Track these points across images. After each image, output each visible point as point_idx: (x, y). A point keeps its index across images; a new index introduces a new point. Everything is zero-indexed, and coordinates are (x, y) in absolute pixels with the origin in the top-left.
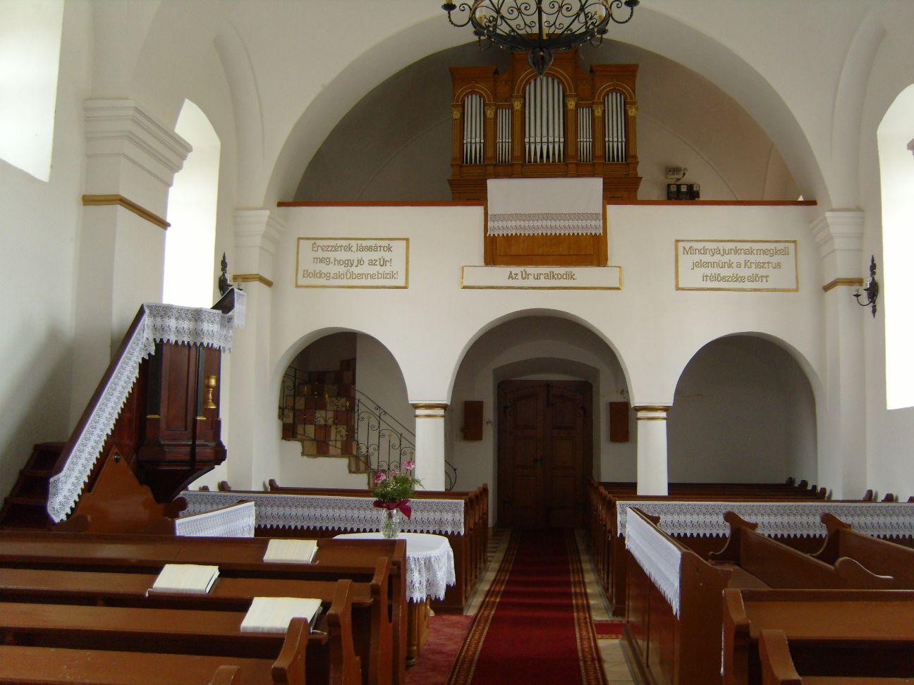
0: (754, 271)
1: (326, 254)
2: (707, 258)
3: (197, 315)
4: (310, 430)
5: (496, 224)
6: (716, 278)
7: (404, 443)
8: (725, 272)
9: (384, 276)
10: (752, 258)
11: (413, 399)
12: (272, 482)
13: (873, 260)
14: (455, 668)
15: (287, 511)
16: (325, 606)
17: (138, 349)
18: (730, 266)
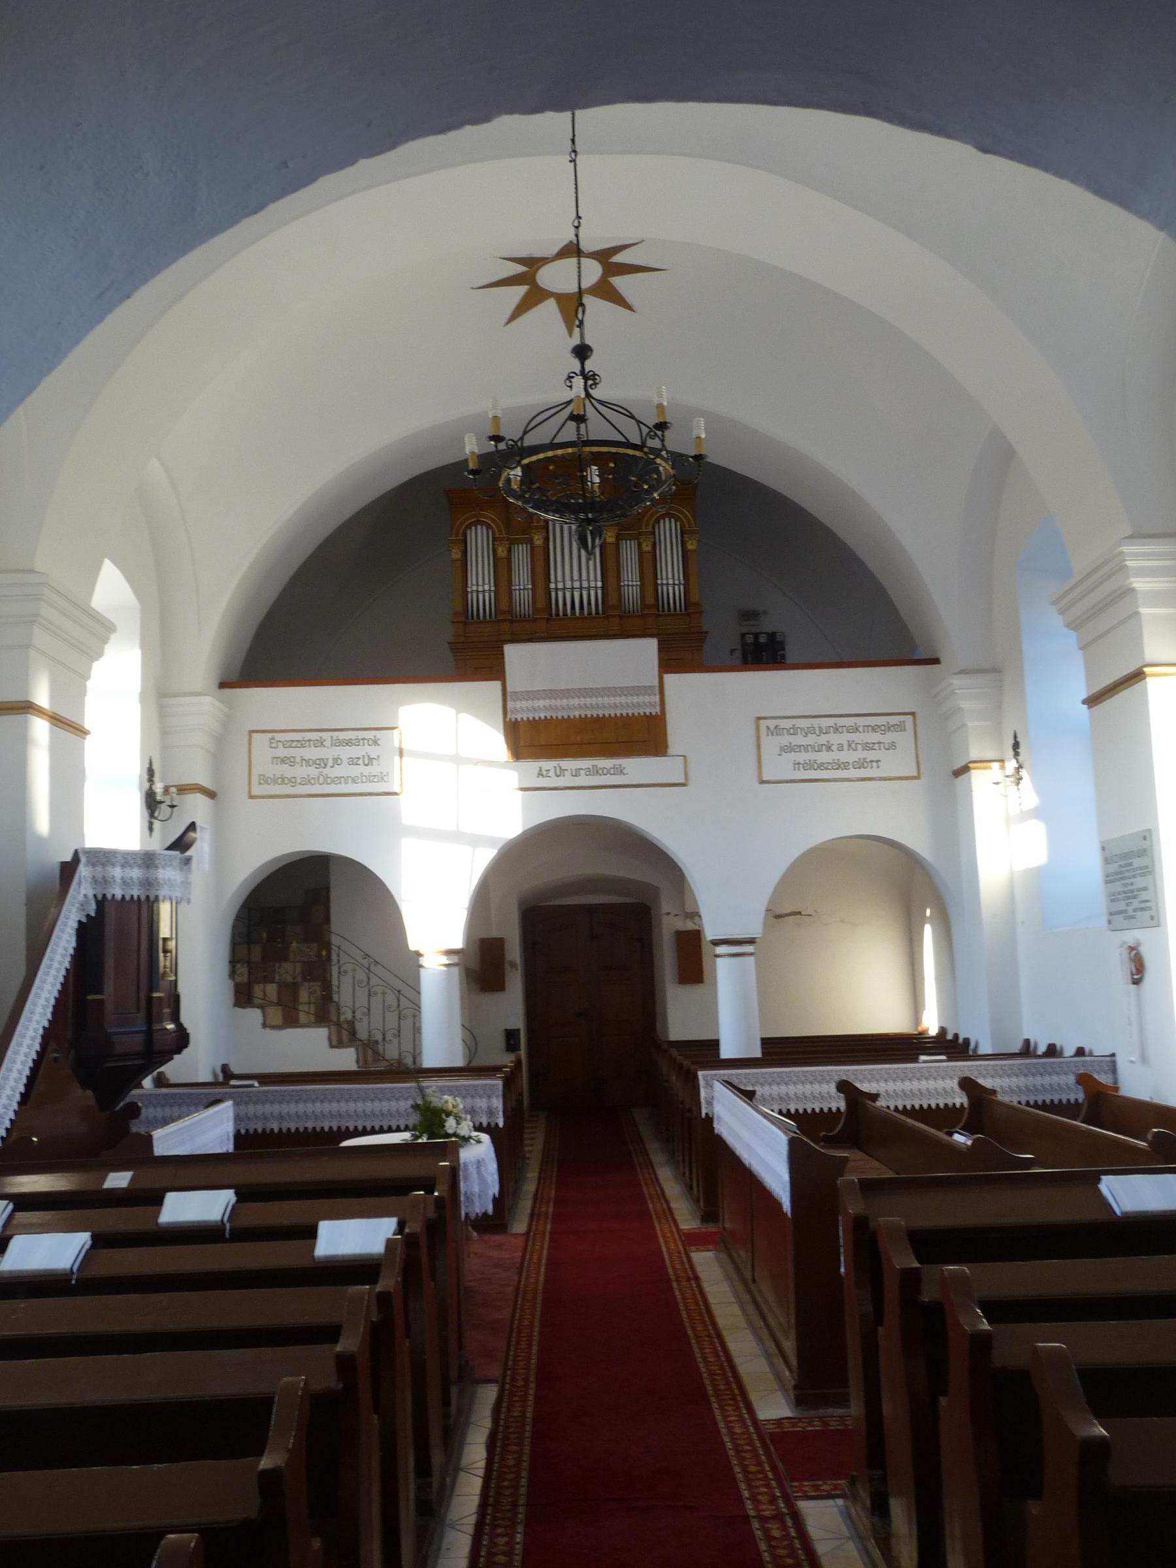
0: (860, 754)
2: (799, 740)
4: (272, 990)
5: (519, 704)
6: (809, 765)
7: (404, 1003)
8: (824, 757)
10: (857, 737)
12: (225, 1068)
13: (1015, 737)
14: (516, 1302)
16: (401, 1226)
17: (74, 910)
18: (829, 749)
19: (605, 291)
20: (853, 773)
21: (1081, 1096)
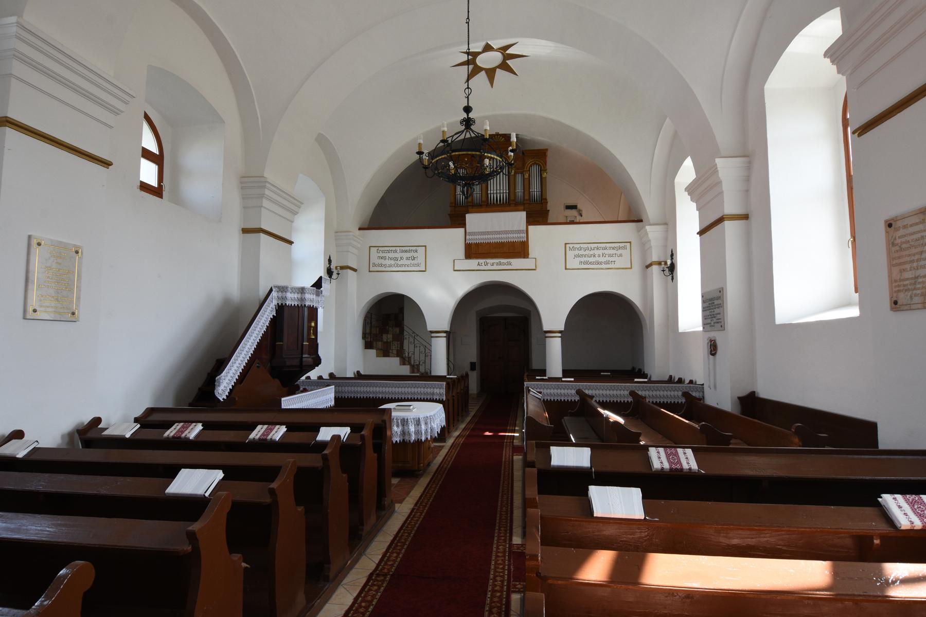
0: (607, 258)
1: (384, 255)
2: (582, 252)
3: (302, 290)
6: (586, 263)
8: (592, 259)
9: (414, 265)
11: (430, 328)
15: (368, 389)
19: (504, 66)
20: (603, 266)
21: (684, 401)
